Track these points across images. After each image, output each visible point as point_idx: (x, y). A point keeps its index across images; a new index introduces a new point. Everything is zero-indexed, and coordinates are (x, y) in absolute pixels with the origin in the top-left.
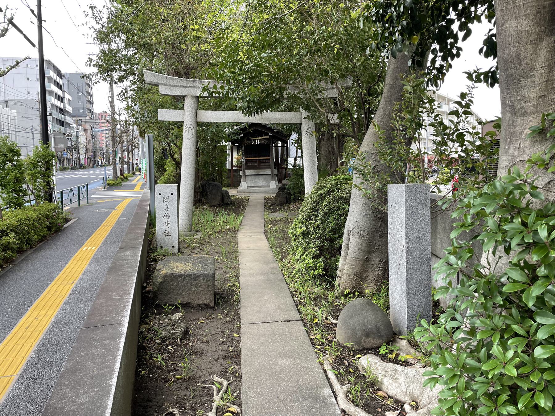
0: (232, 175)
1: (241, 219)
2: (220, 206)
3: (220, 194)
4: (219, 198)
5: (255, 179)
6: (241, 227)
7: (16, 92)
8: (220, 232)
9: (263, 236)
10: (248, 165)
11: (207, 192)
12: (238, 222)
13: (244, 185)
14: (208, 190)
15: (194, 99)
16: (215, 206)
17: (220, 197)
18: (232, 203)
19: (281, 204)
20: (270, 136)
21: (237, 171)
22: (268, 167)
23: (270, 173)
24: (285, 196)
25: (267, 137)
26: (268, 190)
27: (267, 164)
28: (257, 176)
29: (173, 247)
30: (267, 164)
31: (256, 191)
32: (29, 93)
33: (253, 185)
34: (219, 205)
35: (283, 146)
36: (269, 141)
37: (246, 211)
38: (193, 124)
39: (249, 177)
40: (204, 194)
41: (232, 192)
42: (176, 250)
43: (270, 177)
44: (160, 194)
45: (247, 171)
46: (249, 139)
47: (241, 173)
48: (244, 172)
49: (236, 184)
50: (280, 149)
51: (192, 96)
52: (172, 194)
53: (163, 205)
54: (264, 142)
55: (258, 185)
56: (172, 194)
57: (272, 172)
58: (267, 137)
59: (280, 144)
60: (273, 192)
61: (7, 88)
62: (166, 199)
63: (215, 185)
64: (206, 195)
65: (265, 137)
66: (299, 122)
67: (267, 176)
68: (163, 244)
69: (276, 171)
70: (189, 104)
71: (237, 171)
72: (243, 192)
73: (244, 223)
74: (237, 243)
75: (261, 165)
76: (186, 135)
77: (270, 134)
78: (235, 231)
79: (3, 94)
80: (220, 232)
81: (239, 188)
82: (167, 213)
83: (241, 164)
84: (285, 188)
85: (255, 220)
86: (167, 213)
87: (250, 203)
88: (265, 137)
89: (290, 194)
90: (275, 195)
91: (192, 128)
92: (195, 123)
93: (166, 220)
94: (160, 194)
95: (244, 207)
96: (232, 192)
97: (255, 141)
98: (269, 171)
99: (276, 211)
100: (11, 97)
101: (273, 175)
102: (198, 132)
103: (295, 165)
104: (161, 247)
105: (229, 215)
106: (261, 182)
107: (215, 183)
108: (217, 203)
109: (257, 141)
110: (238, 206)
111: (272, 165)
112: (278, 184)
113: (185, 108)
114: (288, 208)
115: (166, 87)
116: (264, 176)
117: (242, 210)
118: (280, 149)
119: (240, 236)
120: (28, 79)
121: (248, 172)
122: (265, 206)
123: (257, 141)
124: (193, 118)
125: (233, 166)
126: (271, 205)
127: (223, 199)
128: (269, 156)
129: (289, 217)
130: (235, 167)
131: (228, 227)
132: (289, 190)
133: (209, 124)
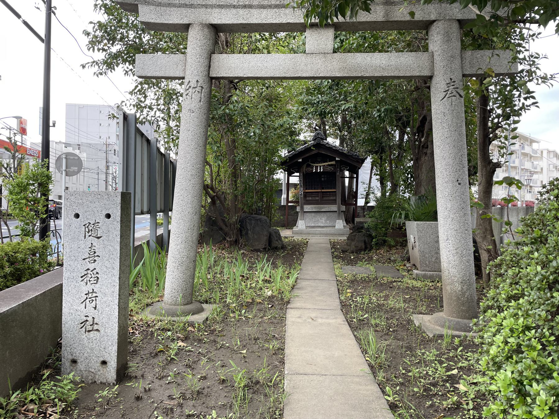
1: (295, 276)
2: (265, 250)
3: (265, 233)
4: (265, 239)
6: (296, 292)
7: (88, 136)
8: (249, 305)
9: (338, 321)
10: (307, 198)
11: (248, 230)
12: (291, 281)
13: (301, 224)
14: (249, 228)
15: (206, 30)
16: (258, 251)
17: (265, 238)
18: (283, 247)
19: (358, 251)
20: (337, 161)
21: (294, 208)
22: (334, 202)
23: (336, 210)
25: (333, 163)
27: (332, 198)
28: (319, 214)
29: (104, 363)
30: (332, 198)
31: (317, 232)
32: (100, 137)
33: (313, 225)
34: (265, 249)
35: (351, 178)
36: (335, 169)
37: (304, 261)
38: (201, 81)
39: (308, 214)
40: (244, 233)
41: (285, 233)
42: (111, 373)
44: (77, 216)
45: (305, 206)
47: (298, 209)
48: (302, 208)
49: (291, 224)
50: (347, 180)
51: (201, 24)
52: (108, 216)
53: (84, 245)
54: (329, 169)
55: (320, 225)
56: (108, 216)
58: (333, 163)
59: (347, 173)
60: (342, 235)
61: (81, 133)
62: (91, 229)
63: (260, 220)
64: (247, 234)
65: (330, 163)
66: (426, 73)
67: (331, 214)
68: (77, 354)
69: (343, 208)
70: (196, 41)
71: (294, 208)
72: (300, 233)
73: (302, 283)
74: (282, 339)
75: (324, 199)
76: (188, 102)
77: (337, 159)
78: (281, 303)
79: (77, 138)
80: (249, 305)
81: (295, 229)
82: (91, 266)
83: (297, 198)
84: (362, 228)
85: (320, 277)
86: (91, 266)
87: (310, 248)
88: (330, 163)
89: (370, 236)
90: (346, 238)
91: (199, 89)
92: (207, 80)
93: (90, 288)
94: (77, 216)
95: (302, 254)
96: (285, 233)
97: (317, 167)
98: (334, 208)
99: (351, 263)
100: (84, 141)
101: (339, 212)
102: (211, 97)
104: (74, 362)
105: (275, 266)
106: (322, 221)
107: (259, 217)
108: (261, 246)
109: (319, 168)
110: (292, 254)
111: (339, 200)
112: (345, 224)
113: (188, 51)
114: (371, 259)
115: (152, 7)
116: (328, 214)
117: (298, 259)
118: (347, 180)
119: (292, 316)
120: (100, 125)
121: (307, 208)
122: (333, 253)
123: (319, 168)
124: (202, 69)
125: (288, 201)
126: (343, 253)
128: (335, 188)
129: (381, 275)
130: (291, 202)
131: (269, 293)
132: (368, 229)
133: (233, 83)
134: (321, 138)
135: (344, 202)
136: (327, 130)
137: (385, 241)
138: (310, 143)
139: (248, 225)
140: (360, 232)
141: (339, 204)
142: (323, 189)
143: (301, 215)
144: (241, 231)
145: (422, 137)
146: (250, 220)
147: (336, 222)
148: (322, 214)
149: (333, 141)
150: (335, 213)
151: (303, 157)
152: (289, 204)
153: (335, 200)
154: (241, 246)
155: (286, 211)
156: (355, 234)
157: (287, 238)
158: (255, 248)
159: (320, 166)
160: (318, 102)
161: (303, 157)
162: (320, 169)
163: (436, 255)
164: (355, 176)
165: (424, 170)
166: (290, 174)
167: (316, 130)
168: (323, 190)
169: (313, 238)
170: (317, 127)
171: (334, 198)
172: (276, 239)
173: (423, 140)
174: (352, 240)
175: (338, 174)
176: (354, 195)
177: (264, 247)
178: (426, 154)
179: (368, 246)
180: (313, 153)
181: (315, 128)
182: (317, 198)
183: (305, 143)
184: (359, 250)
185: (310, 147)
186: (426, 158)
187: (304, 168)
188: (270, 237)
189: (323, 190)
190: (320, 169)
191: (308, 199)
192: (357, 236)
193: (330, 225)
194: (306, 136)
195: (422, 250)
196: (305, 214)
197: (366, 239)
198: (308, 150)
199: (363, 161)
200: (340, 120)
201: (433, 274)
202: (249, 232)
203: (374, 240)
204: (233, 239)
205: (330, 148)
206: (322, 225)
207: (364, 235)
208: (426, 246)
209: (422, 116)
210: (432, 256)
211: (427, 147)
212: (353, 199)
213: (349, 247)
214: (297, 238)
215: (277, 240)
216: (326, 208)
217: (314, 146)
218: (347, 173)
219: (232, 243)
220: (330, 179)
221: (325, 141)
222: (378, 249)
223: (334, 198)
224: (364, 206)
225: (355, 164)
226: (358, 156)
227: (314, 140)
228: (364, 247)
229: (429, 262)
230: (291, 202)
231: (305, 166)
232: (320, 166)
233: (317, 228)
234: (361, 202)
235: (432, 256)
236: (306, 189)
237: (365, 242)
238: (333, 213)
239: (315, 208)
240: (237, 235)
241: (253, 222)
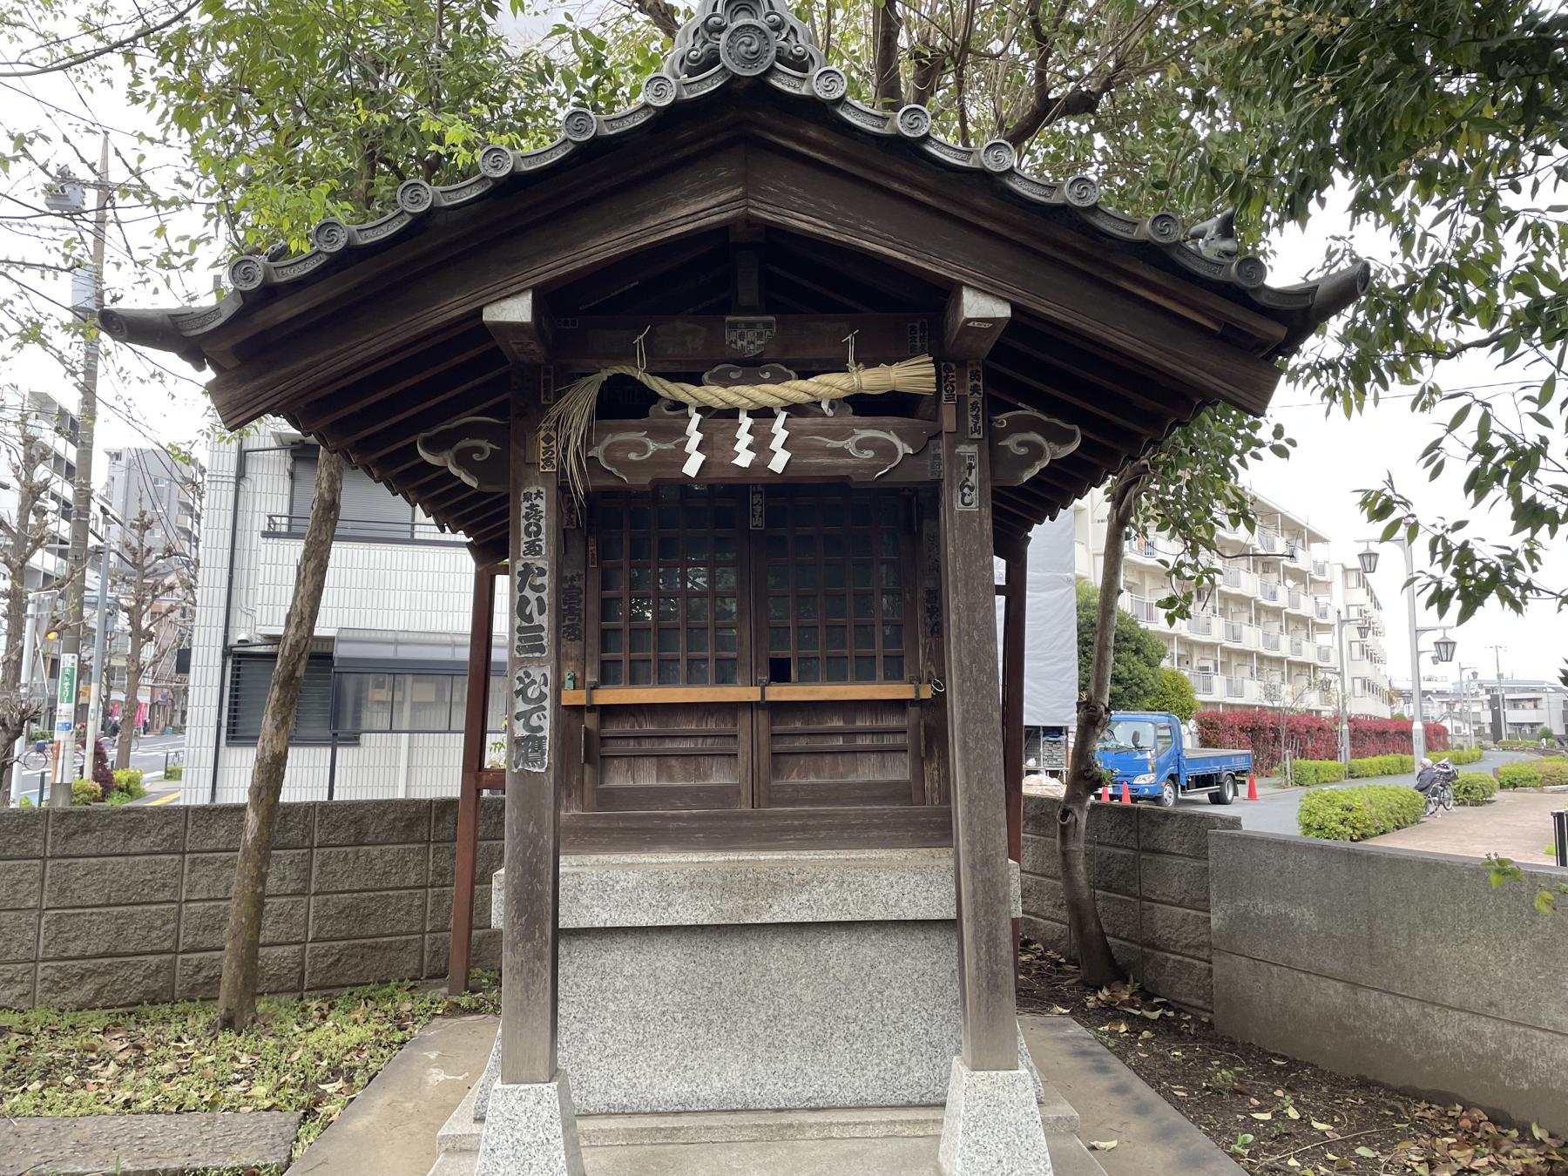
25: (910, 374)
39: (618, 956)
46: (624, 402)
67: (869, 949)
75: (777, 788)
77: (977, 306)
109: (754, 423)
116: (835, 949)
123: (754, 423)
142: (780, 672)
148: (779, 956)
162: (761, 445)
182: (719, 777)
190: (761, 445)
191: (619, 779)
193: (865, 1085)
231: (580, 404)
232: (763, 414)
239: (696, 883)
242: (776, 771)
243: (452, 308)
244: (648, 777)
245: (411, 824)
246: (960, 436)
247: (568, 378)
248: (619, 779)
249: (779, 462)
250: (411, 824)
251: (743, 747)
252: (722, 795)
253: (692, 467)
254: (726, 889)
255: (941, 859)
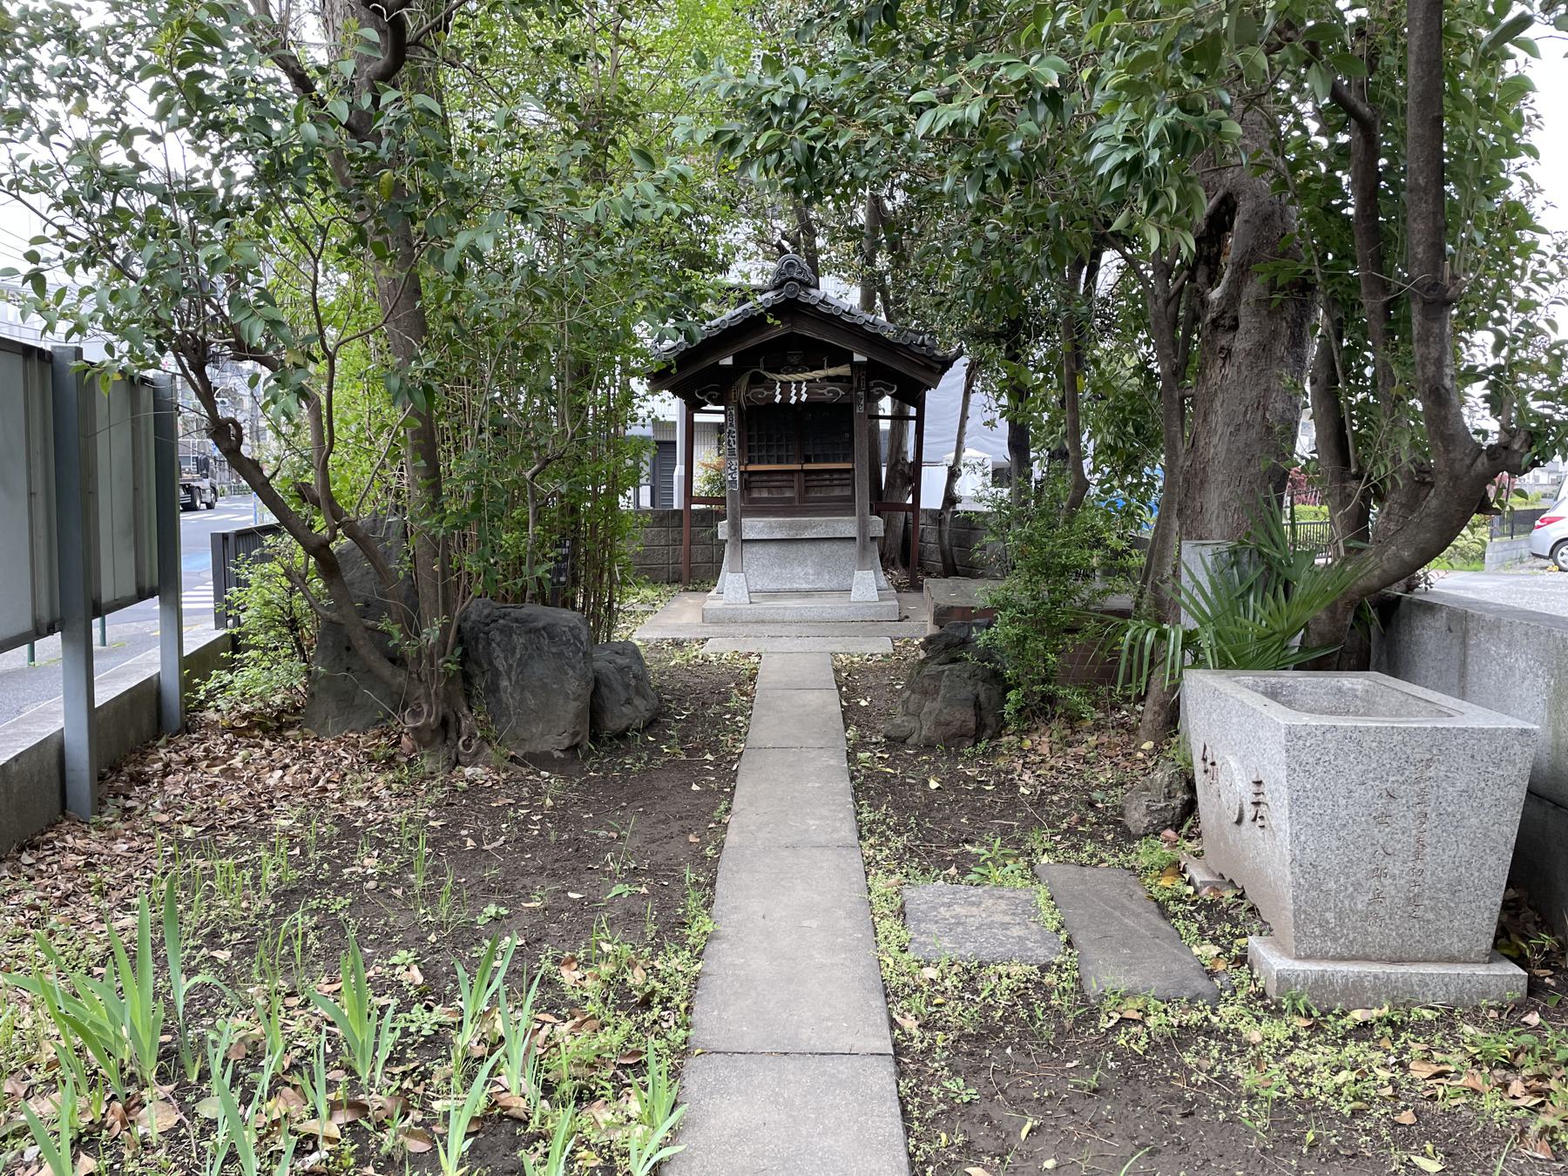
0: (685, 536)
3: (573, 685)
4: (568, 710)
5: (850, 914)
10: (754, 493)
13: (732, 588)
14: (501, 664)
16: (540, 760)
17: (573, 706)
20: (856, 366)
21: (709, 519)
22: (845, 506)
24: (967, 692)
25: (844, 370)
26: (842, 613)
27: (837, 492)
28: (794, 547)
30: (837, 492)
33: (774, 586)
34: (572, 749)
35: (899, 418)
39: (756, 548)
40: (480, 683)
43: (853, 549)
45: (747, 522)
46: (757, 380)
48: (736, 529)
57: (863, 526)
58: (844, 370)
63: (549, 631)
64: (493, 689)
65: (832, 372)
67: (835, 546)
69: (877, 525)
75: (809, 495)
77: (857, 358)
88: (832, 372)
97: (786, 386)
98: (846, 526)
101: (864, 540)
103: (950, 499)
106: (802, 572)
108: (554, 742)
109: (796, 387)
111: (862, 498)
116: (825, 547)
121: (754, 527)
123: (796, 387)
127: (595, 711)
128: (848, 456)
130: (700, 500)
134: (801, 282)
135: (880, 503)
136: (820, 251)
137: (1050, 699)
138: (760, 298)
139: (498, 652)
140: (954, 661)
141: (862, 515)
142: (808, 460)
143: (733, 554)
144: (467, 678)
145: (1212, 282)
146: (507, 632)
147: (851, 575)
148: (806, 548)
149: (839, 291)
150: (850, 545)
151: (737, 349)
152: (694, 507)
153: (851, 499)
154: (467, 746)
155: (685, 529)
156: (932, 668)
157: (678, 644)
158: (528, 748)
159: (799, 383)
160: (794, 99)
161: (737, 349)
162: (798, 394)
163: (1375, 882)
164: (913, 411)
165: (1218, 419)
166: (693, 406)
167: (783, 250)
168: (807, 467)
169: (779, 645)
170: (785, 243)
171: (847, 492)
172: (623, 695)
173: (1215, 294)
174: (925, 693)
175: (860, 410)
176: (910, 476)
177: (567, 743)
178: (1228, 353)
179: (990, 720)
180: (772, 335)
181: (780, 246)
182: (788, 494)
183: (744, 300)
184: (954, 736)
185: (762, 317)
186: (1227, 371)
187: (742, 390)
188: (595, 693)
189: (807, 467)
190: (798, 394)
191: (755, 494)
192: (945, 681)
193: (834, 585)
194: (751, 271)
195: (1310, 855)
196: (747, 548)
197: (981, 690)
198: (752, 324)
199: (947, 364)
200: (861, 216)
201: (1360, 978)
202: (505, 683)
203: (1012, 695)
204: (428, 717)
205: (832, 319)
206: (805, 586)
207: (973, 675)
208: (1330, 840)
209: (1220, 193)
210: (1357, 886)
211: (1234, 327)
212: (904, 485)
213: (914, 724)
214: (720, 648)
215: (629, 702)
216: (820, 526)
217: (776, 310)
218: (886, 405)
219: (427, 737)
220: (829, 426)
221: (813, 292)
222: (1028, 732)
223: (847, 492)
224: (940, 513)
225: (920, 376)
226: (930, 349)
227: (777, 287)
228: (972, 725)
229: (1340, 916)
230: (700, 500)
231: (744, 381)
232: (799, 383)
233: (783, 620)
234: (931, 496)
235: (1357, 886)
236: (751, 462)
237: (977, 706)
238: (842, 545)
239: (781, 526)
240: (448, 700)
241: (519, 641)
242: (807, 492)
243: (710, 361)
244: (765, 494)
245: (662, 519)
246: (858, 389)
247: (744, 371)
248: (755, 494)
249: (803, 398)
250: (662, 519)
251: (796, 485)
252: (790, 499)
253: (777, 400)
254: (790, 528)
255: (855, 518)
